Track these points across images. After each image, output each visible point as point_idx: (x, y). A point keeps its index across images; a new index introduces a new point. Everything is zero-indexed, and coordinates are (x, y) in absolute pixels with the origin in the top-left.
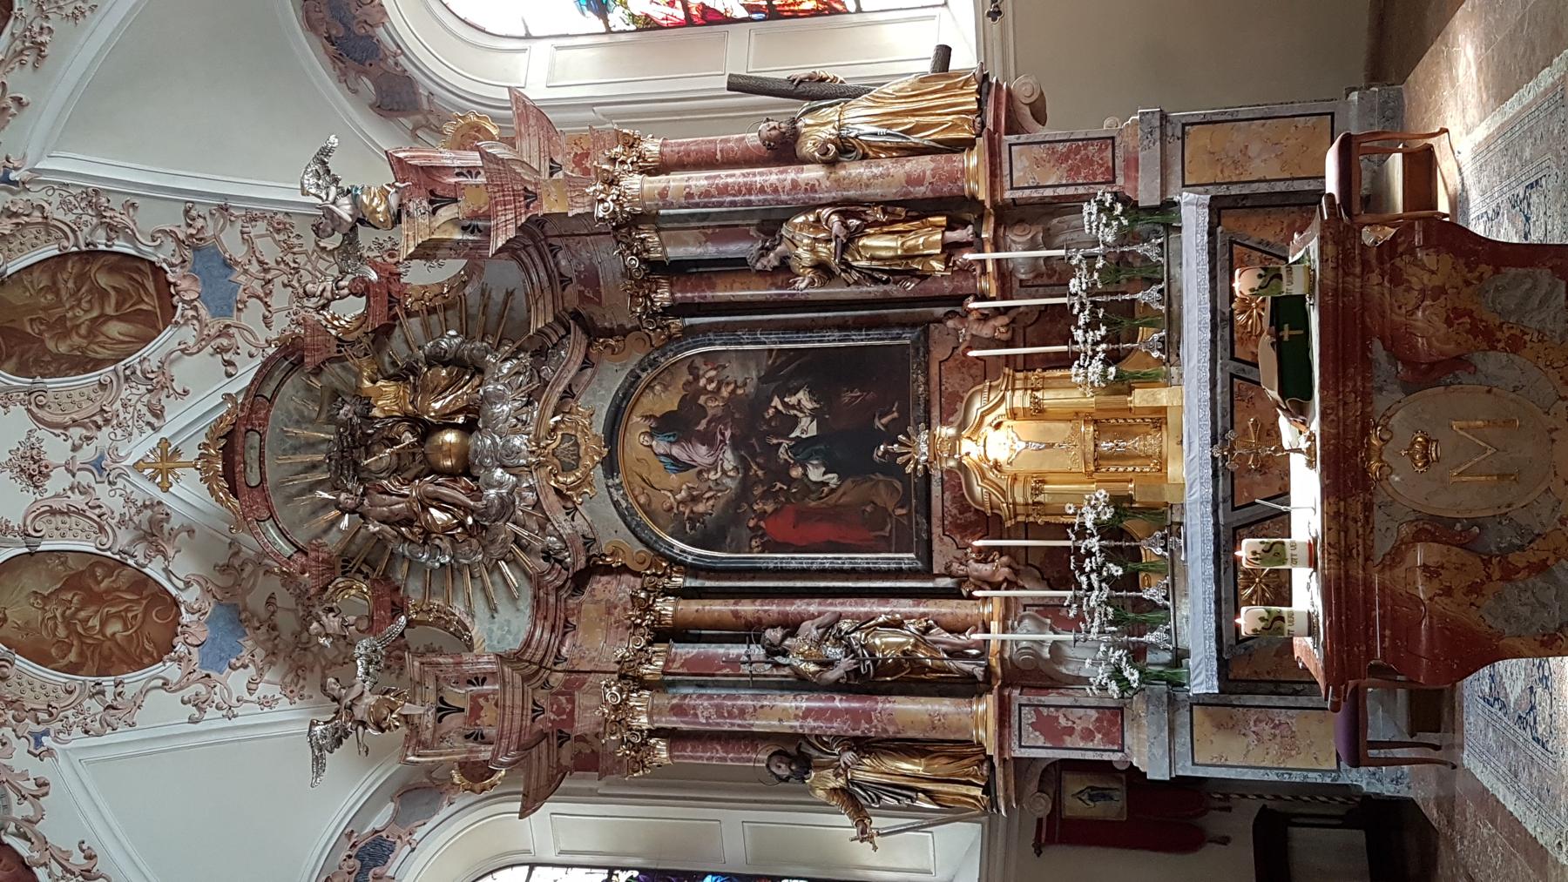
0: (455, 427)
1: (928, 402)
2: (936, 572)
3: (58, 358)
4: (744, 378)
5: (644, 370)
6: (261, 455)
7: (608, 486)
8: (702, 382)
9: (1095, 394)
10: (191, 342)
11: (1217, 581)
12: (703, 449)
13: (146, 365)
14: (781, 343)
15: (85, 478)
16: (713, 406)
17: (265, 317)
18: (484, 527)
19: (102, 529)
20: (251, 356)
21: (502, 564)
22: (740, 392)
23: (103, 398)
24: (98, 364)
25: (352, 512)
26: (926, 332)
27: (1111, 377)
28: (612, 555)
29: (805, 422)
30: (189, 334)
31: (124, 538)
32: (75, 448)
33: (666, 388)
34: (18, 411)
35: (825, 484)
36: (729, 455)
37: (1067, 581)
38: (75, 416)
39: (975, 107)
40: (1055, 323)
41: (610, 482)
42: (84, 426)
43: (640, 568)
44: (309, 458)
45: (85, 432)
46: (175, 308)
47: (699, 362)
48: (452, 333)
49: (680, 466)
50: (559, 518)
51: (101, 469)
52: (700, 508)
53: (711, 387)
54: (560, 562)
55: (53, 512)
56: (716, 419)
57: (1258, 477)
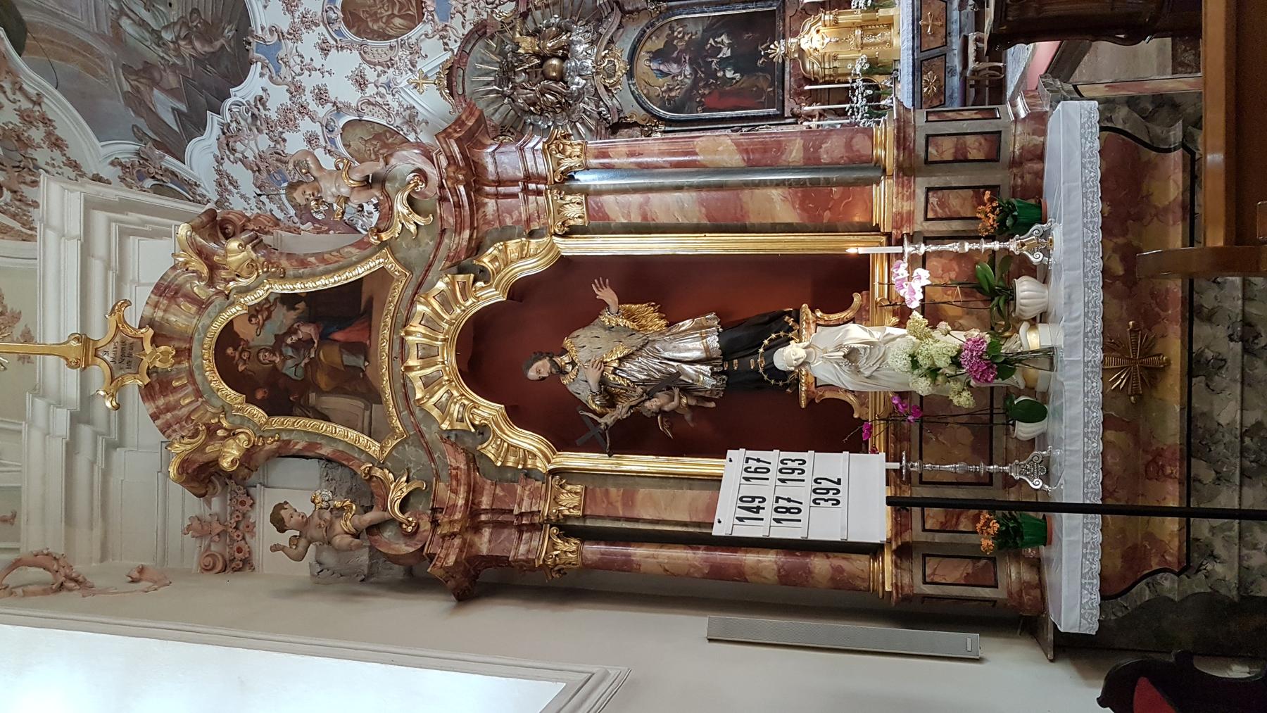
0: (557, 57)
2: (786, 116)
3: (373, 31)
5: (648, 28)
6: (463, 79)
7: (629, 84)
8: (676, 34)
10: (430, 32)
11: (914, 84)
12: (675, 66)
13: (410, 40)
14: (714, 12)
15: (382, 90)
16: (681, 45)
17: (463, 23)
18: (570, 105)
19: (389, 116)
20: (456, 41)
21: (578, 124)
22: (694, 37)
23: (391, 54)
24: (390, 37)
25: (509, 97)
28: (630, 117)
29: (725, 49)
30: (428, 28)
31: (399, 121)
32: (379, 76)
33: (658, 37)
34: (356, 53)
35: (734, 79)
36: (688, 68)
37: (849, 100)
39: (989, 411)
41: (630, 82)
43: (644, 123)
44: (486, 79)
45: (382, 68)
46: (424, 14)
47: (674, 24)
48: (556, 16)
49: (664, 74)
50: (606, 98)
51: (390, 87)
52: (673, 94)
54: (605, 119)
55: (369, 103)
56: (681, 51)
57: (932, 38)
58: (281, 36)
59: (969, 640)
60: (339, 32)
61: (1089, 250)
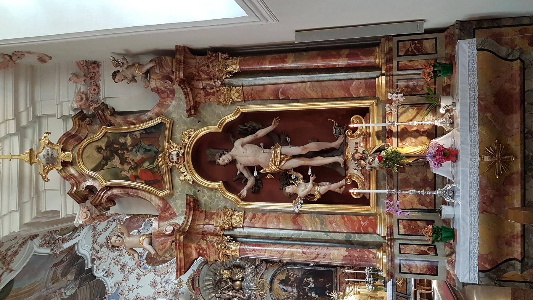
0: (239, 281)
1: (337, 284)
3: (160, 261)
4: (299, 274)
6: (199, 281)
8: (290, 274)
9: (371, 291)
12: (290, 288)
15: (164, 285)
16: (292, 279)
19: (167, 295)
22: (298, 277)
24: (167, 261)
26: (336, 269)
27: (374, 289)
29: (311, 284)
32: (162, 279)
33: (282, 274)
34: (152, 273)
36: (295, 289)
38: (163, 273)
40: (364, 276)
41: (271, 294)
42: (164, 274)
47: (289, 270)
49: (286, 291)
51: (167, 282)
53: (292, 275)
58: (119, 284)
59: (418, 29)
60: (145, 268)
61: (473, 185)
